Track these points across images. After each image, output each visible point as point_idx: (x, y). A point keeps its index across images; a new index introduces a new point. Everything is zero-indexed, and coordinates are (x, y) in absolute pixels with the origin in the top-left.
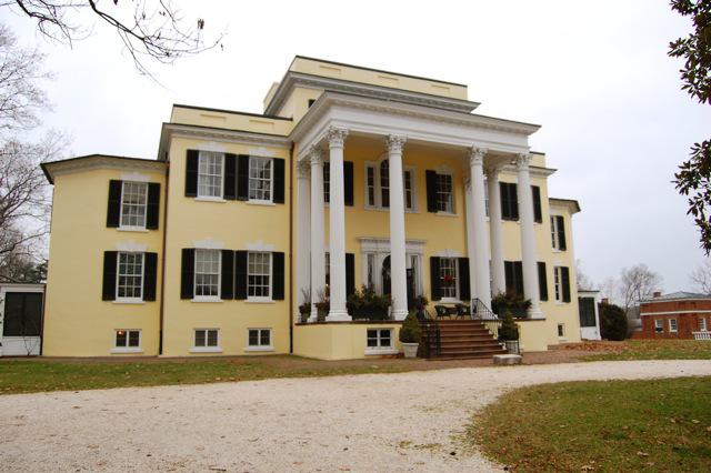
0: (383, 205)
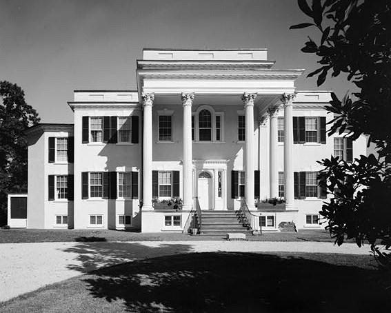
0: (240, 139)
